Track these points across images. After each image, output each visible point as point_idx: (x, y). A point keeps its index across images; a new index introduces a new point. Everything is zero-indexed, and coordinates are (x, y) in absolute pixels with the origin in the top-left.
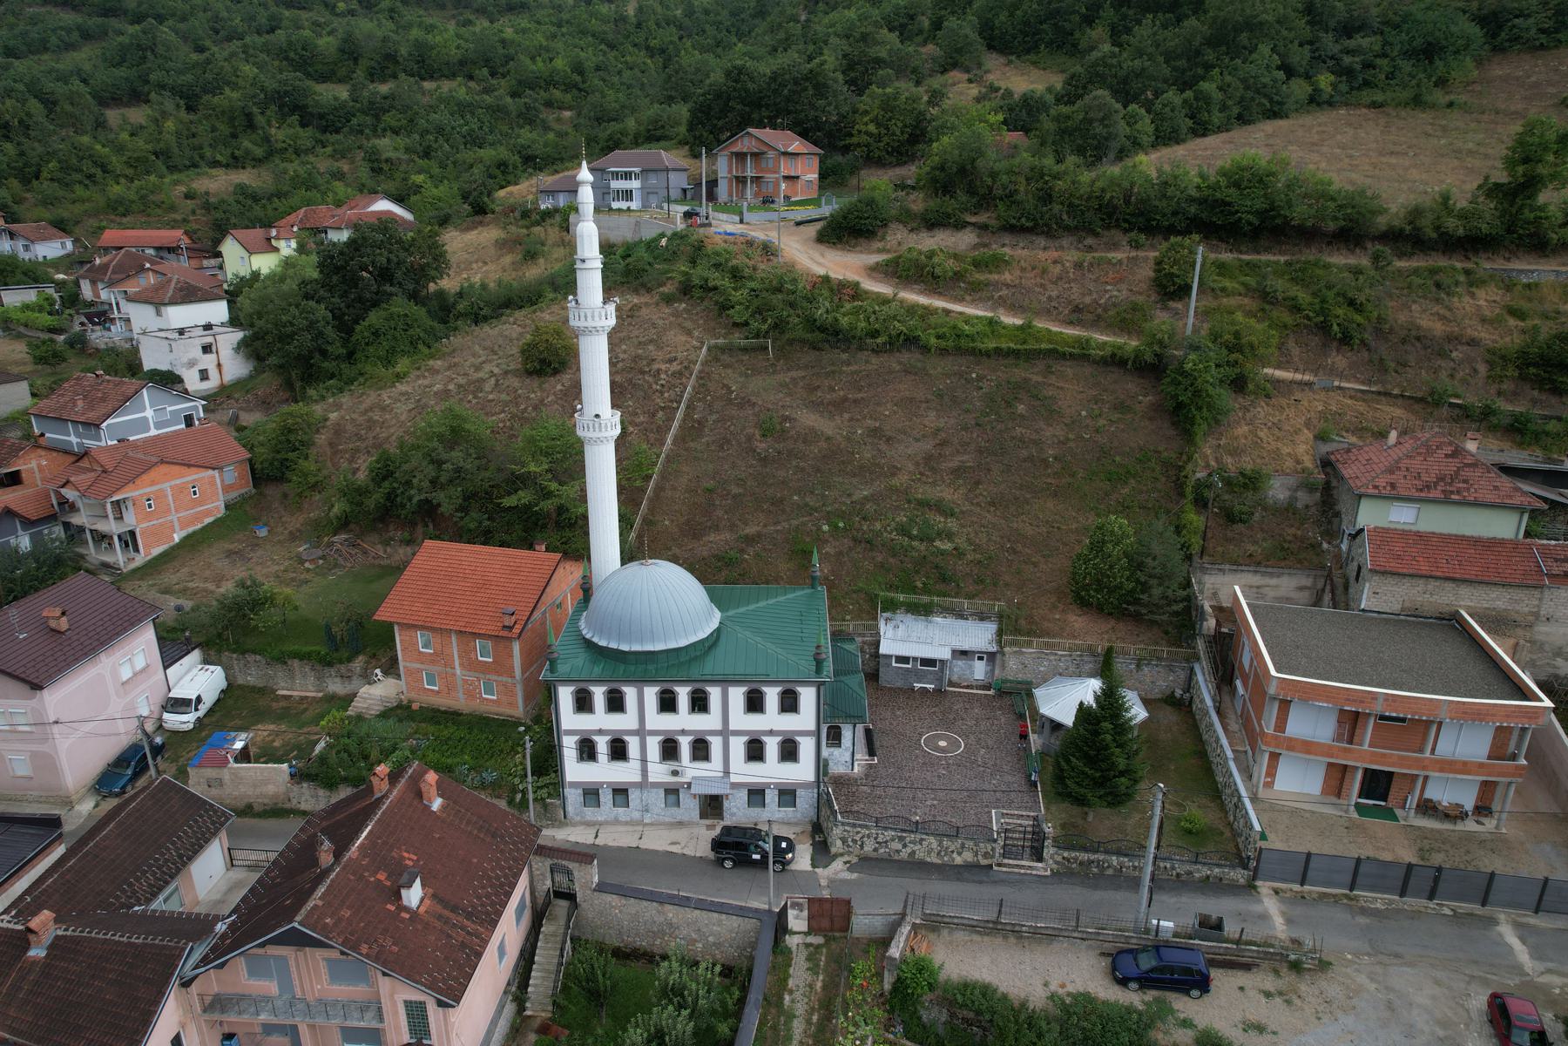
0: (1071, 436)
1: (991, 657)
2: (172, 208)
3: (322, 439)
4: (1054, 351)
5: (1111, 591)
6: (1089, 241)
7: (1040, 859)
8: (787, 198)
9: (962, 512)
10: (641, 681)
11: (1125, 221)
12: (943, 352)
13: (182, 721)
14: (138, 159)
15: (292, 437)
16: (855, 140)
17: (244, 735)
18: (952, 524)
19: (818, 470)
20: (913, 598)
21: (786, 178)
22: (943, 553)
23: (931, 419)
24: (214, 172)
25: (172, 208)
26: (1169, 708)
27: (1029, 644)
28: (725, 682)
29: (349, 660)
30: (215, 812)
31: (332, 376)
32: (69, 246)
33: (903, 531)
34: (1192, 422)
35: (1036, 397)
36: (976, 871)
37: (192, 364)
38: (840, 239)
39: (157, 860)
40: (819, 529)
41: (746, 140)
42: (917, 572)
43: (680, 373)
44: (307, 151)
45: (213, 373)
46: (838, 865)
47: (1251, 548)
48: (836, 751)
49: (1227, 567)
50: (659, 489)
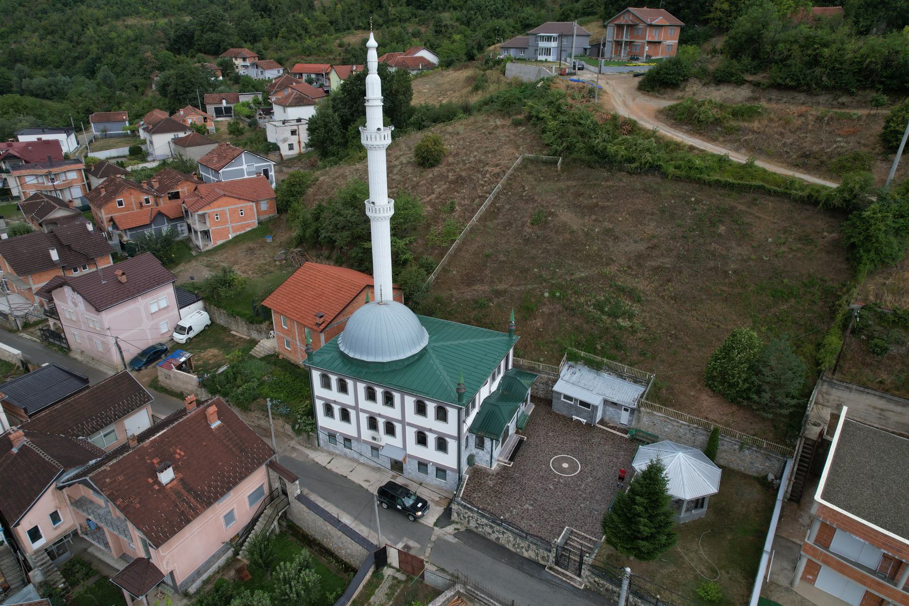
0: (753, 257)
1: (633, 410)
2: (331, 52)
3: (310, 191)
4: (762, 187)
5: (731, 386)
6: (843, 99)
7: (579, 575)
8: (648, 57)
9: (648, 301)
10: (357, 378)
11: (882, 83)
12: (677, 179)
13: (181, 338)
14: (322, 26)
15: (293, 189)
16: (711, 15)
17: (188, 355)
18: (636, 309)
19: (558, 254)
20: (591, 356)
21: (649, 43)
22: (620, 328)
23: (651, 228)
24: (356, 32)
25: (331, 52)
26: (758, 486)
27: (660, 410)
28: (404, 391)
29: (261, 323)
30: (144, 395)
31: (334, 155)
32: (281, 71)
33: (599, 306)
34: (859, 261)
35: (735, 222)
36: (533, 567)
37: (285, 140)
38: (653, 88)
39: (102, 414)
40: (543, 294)
41: (626, 15)
42: (600, 338)
43: (498, 174)
44: (405, 21)
45: (296, 146)
46: (450, 529)
47: (884, 376)
48: (481, 452)
49: (855, 387)
50: (458, 250)
